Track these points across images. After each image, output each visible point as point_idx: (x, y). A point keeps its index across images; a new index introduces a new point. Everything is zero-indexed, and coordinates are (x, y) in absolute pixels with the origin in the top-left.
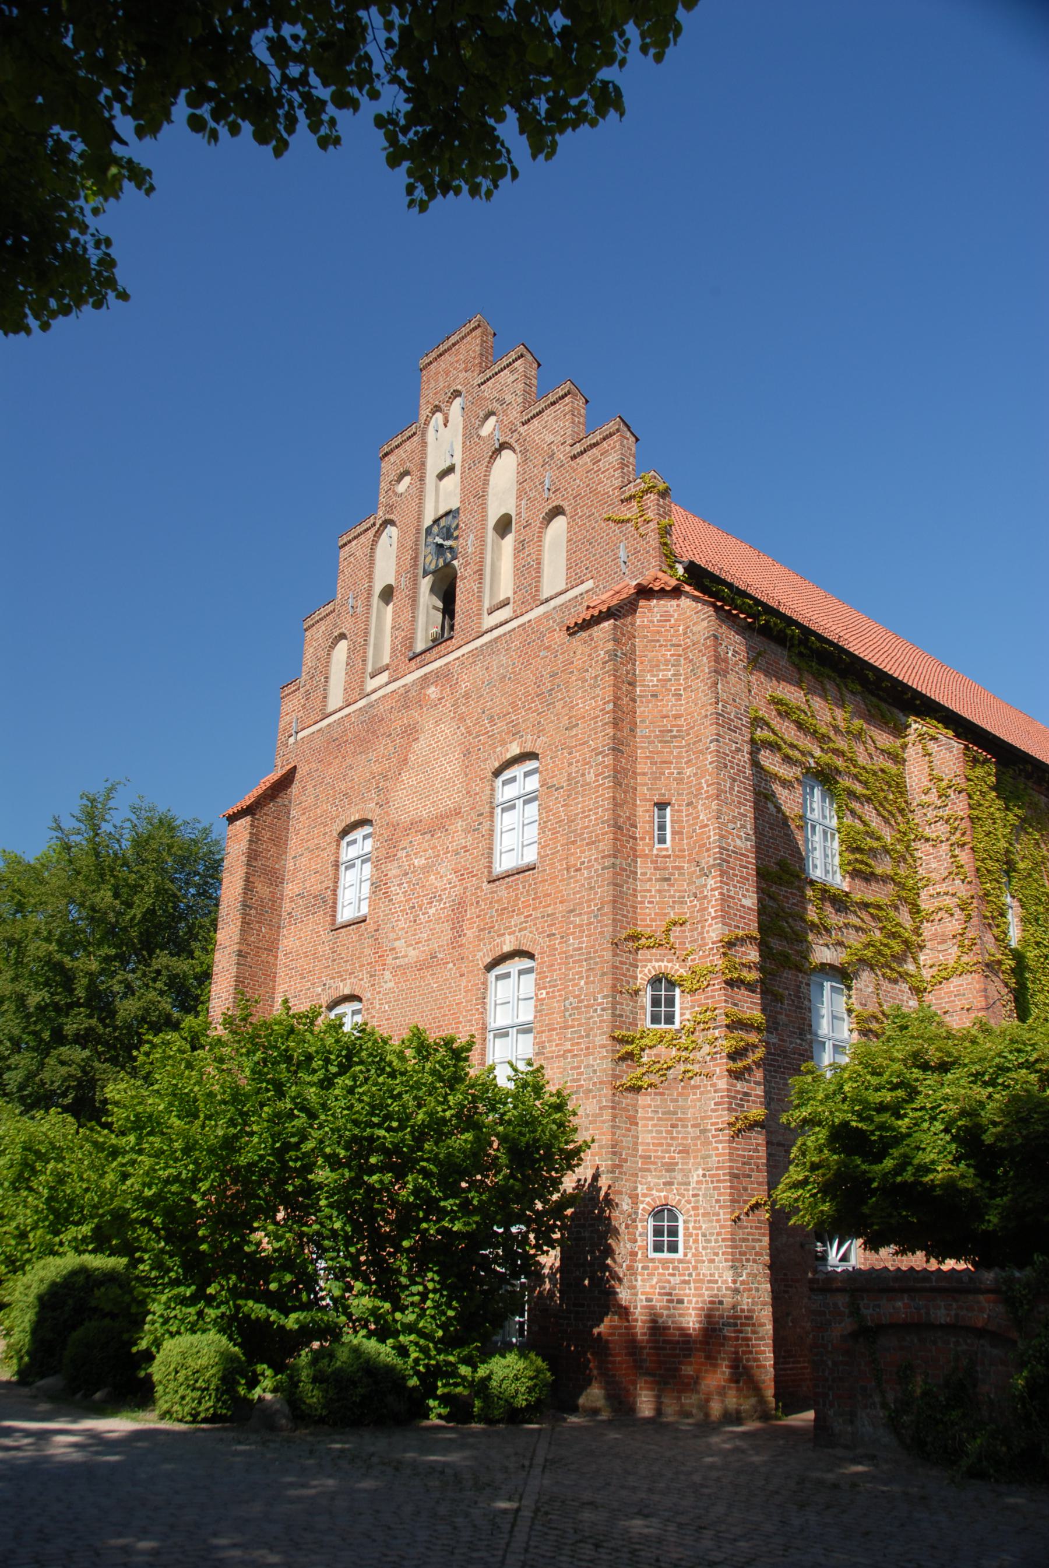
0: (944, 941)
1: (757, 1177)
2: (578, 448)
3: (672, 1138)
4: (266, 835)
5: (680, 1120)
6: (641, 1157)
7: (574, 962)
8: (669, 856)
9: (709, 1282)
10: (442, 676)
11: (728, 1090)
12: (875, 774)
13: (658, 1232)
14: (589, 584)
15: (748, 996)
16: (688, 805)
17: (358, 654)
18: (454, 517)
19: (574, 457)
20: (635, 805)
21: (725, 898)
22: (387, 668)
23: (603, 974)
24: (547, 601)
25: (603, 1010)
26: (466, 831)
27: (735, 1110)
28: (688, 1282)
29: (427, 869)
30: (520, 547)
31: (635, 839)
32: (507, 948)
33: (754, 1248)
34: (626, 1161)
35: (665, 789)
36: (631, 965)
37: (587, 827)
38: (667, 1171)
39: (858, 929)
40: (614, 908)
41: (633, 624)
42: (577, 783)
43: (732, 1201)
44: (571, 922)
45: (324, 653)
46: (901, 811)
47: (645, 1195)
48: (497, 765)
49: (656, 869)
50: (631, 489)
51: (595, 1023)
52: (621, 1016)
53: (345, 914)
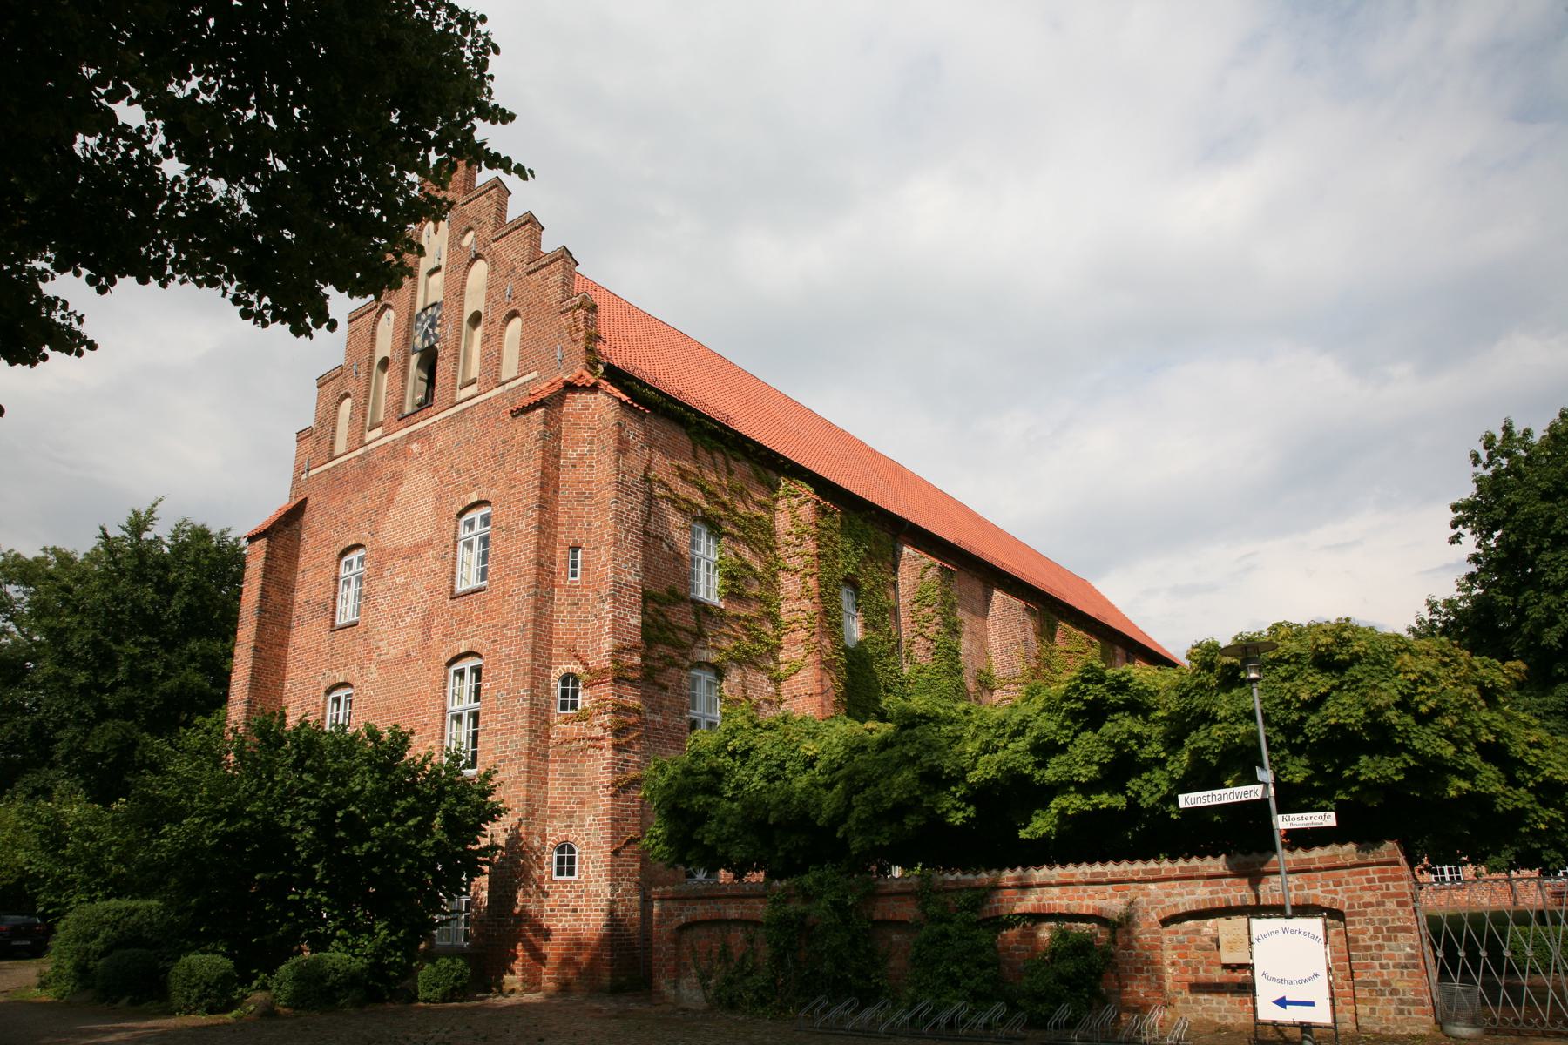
0: (795, 644)
1: (632, 820)
2: (532, 266)
3: (573, 793)
4: (280, 553)
5: (579, 780)
6: (550, 807)
7: (505, 664)
8: (578, 587)
9: (595, 896)
10: (423, 436)
11: (612, 759)
12: (750, 520)
13: (560, 861)
14: (534, 374)
15: (631, 690)
16: (594, 549)
17: (360, 410)
18: (438, 309)
19: (529, 273)
20: (555, 548)
21: (616, 619)
22: (381, 424)
23: (525, 674)
24: (504, 384)
25: (524, 700)
26: (436, 558)
27: (617, 773)
28: (580, 897)
29: (405, 586)
30: (486, 339)
31: (554, 573)
32: (462, 650)
33: (628, 871)
34: (538, 810)
35: (578, 536)
36: (546, 667)
37: (518, 564)
38: (568, 817)
39: (729, 636)
40: (535, 625)
41: (560, 412)
42: (513, 530)
43: (612, 838)
44: (504, 635)
45: (332, 408)
46: (770, 548)
47: (551, 835)
48: (461, 508)
49: (568, 596)
50: (568, 304)
51: (518, 710)
52: (537, 705)
53: (339, 622)
